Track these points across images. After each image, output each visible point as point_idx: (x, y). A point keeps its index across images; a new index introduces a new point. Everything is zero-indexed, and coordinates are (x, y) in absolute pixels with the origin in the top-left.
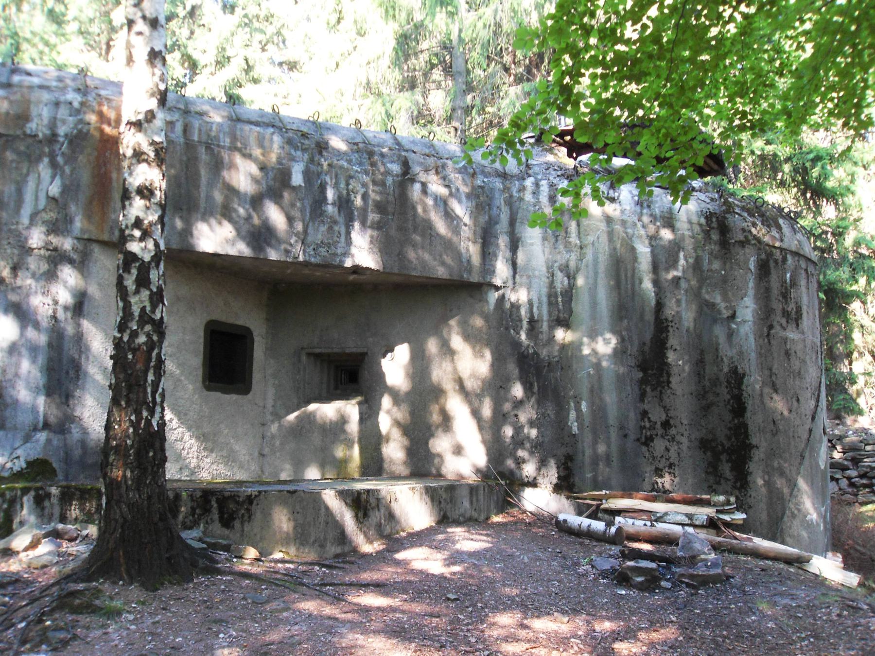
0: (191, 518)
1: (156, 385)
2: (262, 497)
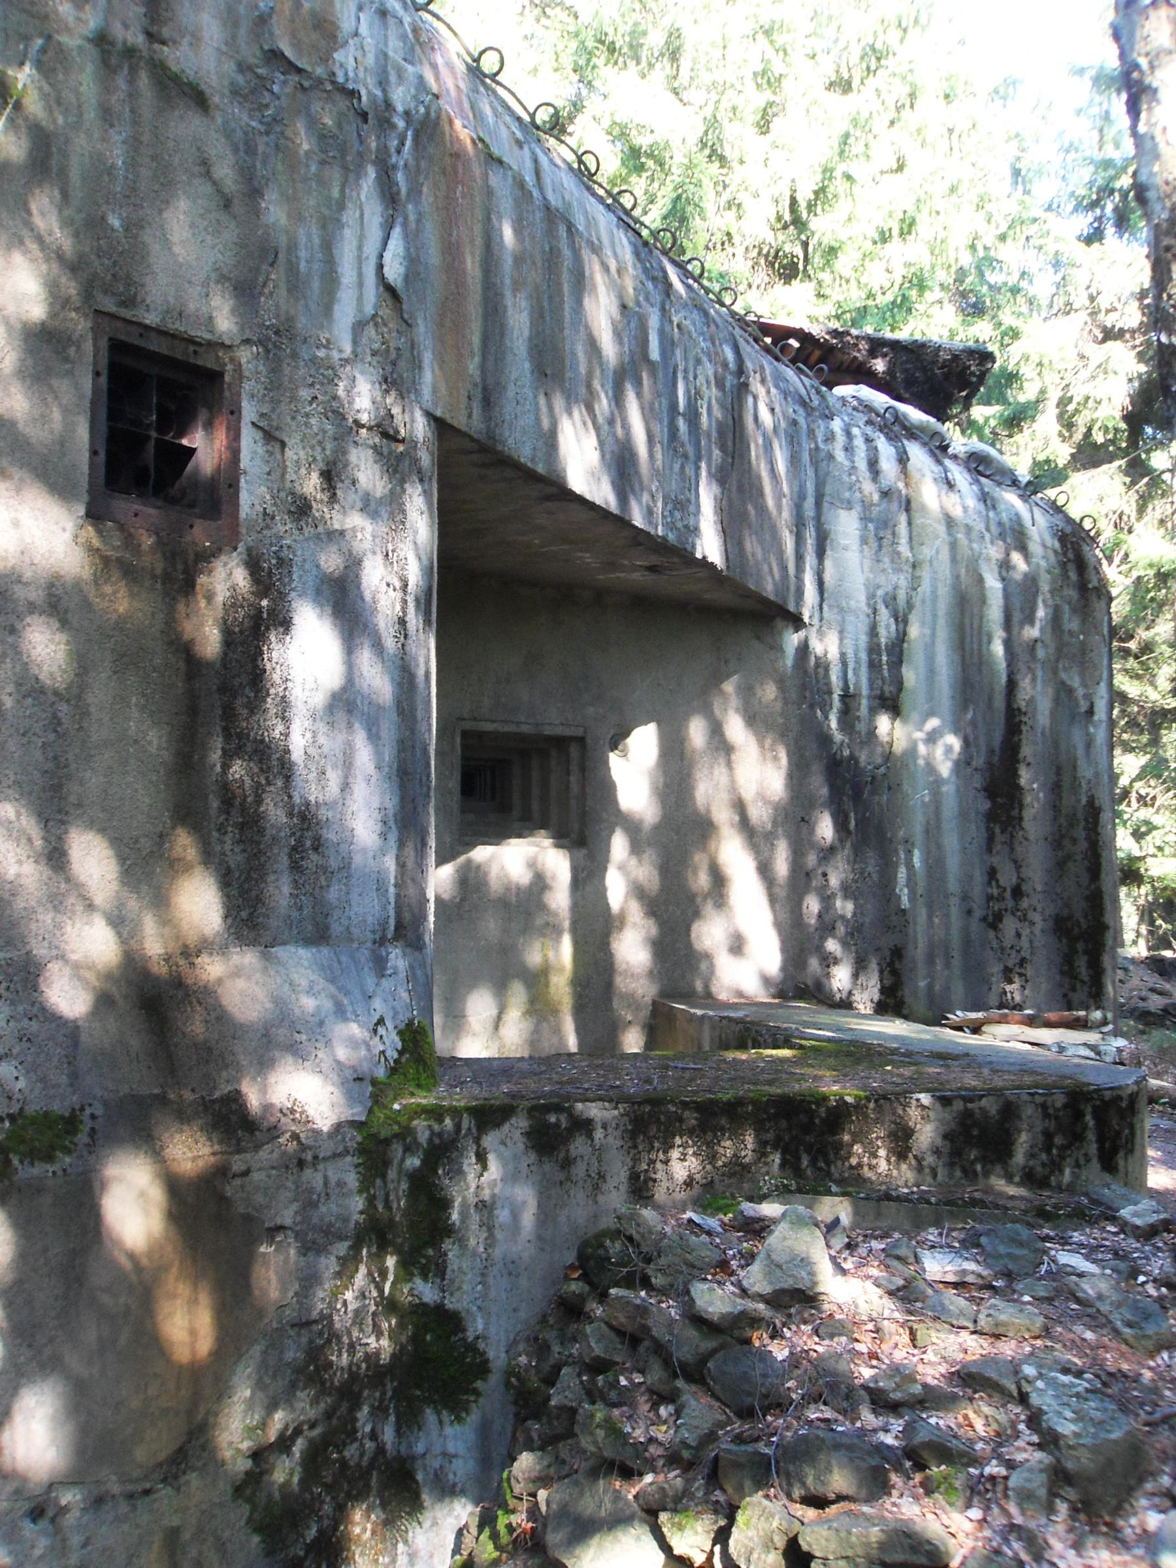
0: (1044, 1156)
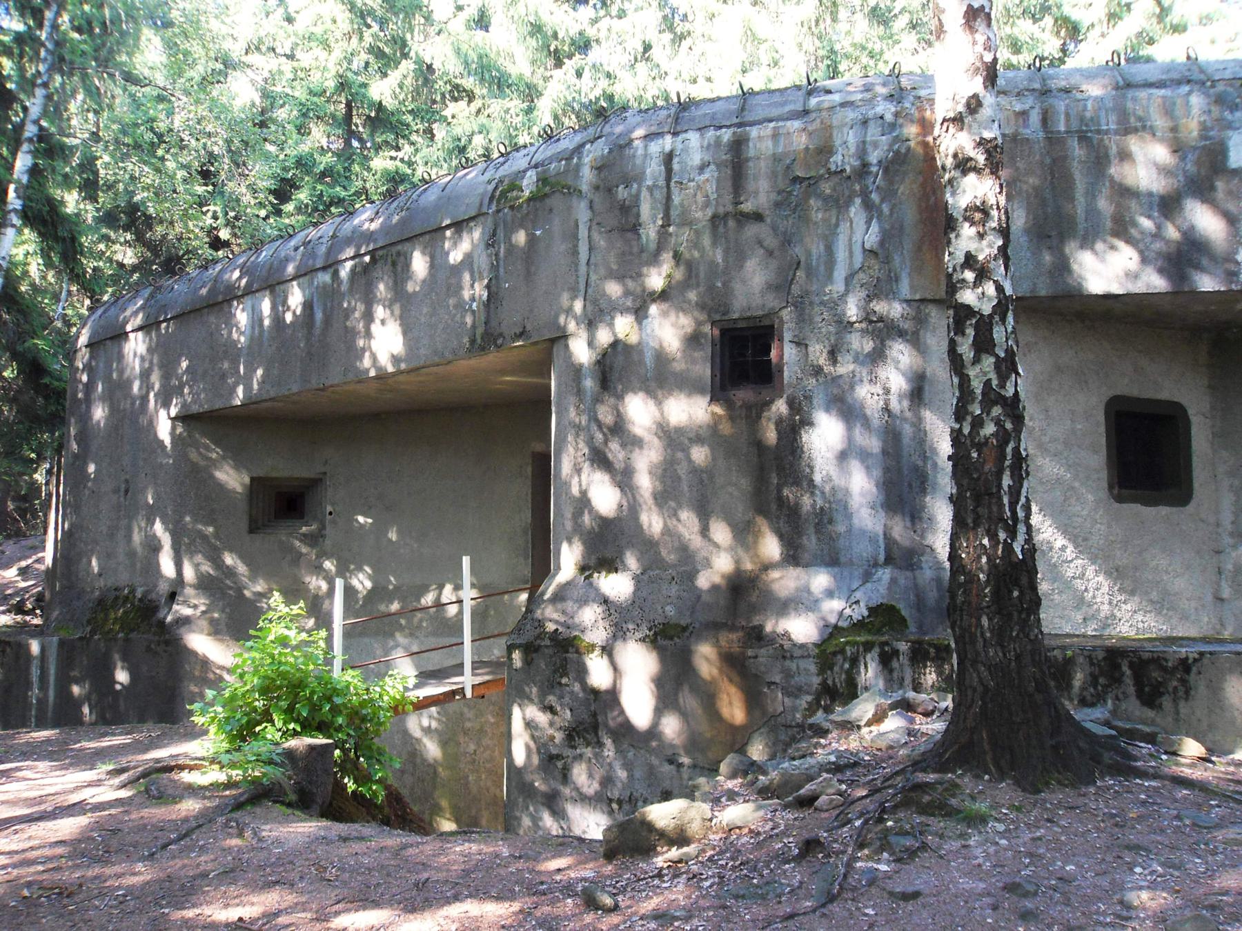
0: (1092, 690)
1: (1015, 493)
2: (1205, 661)
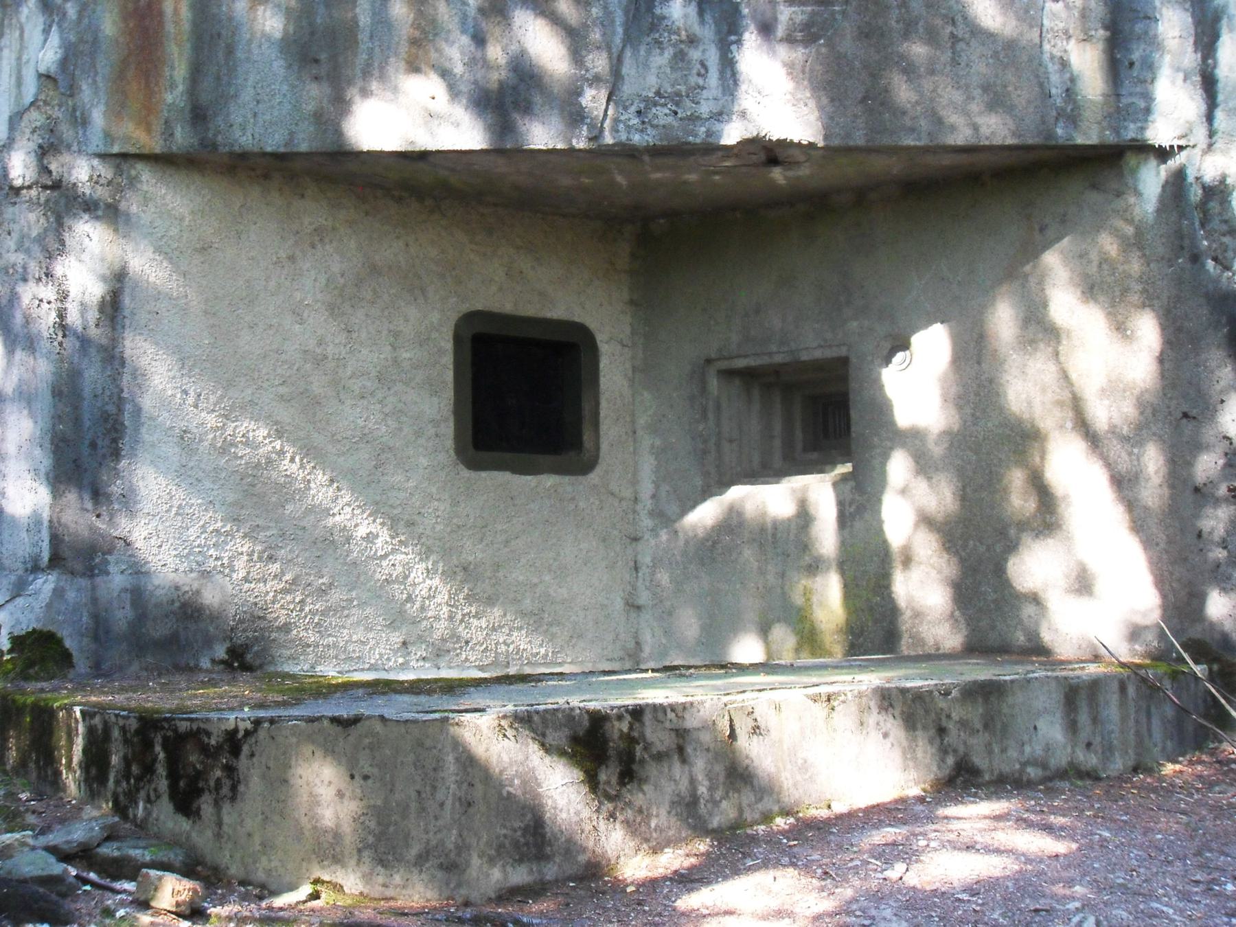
2: (262, 734)
